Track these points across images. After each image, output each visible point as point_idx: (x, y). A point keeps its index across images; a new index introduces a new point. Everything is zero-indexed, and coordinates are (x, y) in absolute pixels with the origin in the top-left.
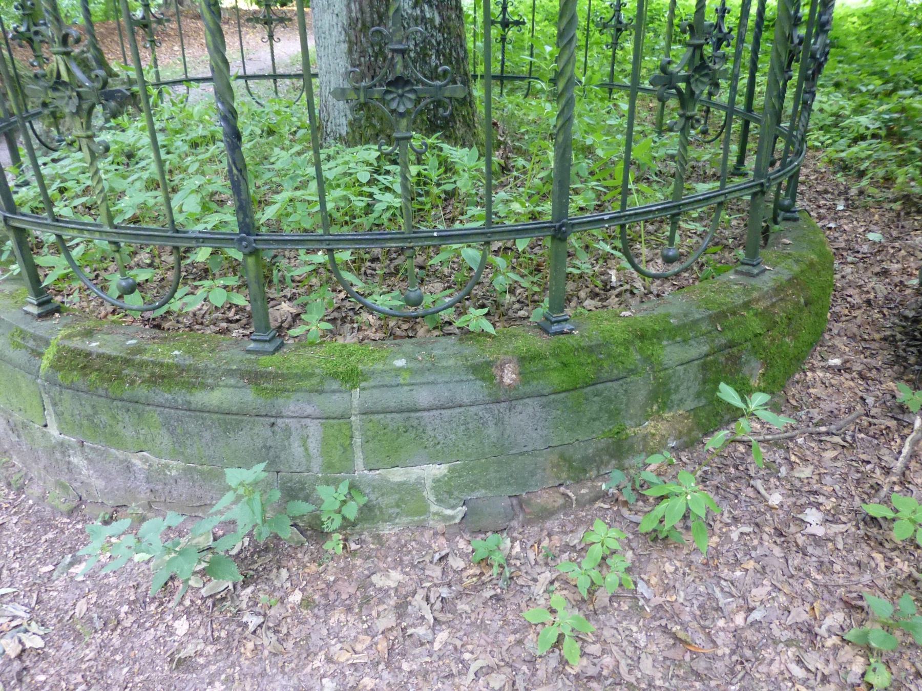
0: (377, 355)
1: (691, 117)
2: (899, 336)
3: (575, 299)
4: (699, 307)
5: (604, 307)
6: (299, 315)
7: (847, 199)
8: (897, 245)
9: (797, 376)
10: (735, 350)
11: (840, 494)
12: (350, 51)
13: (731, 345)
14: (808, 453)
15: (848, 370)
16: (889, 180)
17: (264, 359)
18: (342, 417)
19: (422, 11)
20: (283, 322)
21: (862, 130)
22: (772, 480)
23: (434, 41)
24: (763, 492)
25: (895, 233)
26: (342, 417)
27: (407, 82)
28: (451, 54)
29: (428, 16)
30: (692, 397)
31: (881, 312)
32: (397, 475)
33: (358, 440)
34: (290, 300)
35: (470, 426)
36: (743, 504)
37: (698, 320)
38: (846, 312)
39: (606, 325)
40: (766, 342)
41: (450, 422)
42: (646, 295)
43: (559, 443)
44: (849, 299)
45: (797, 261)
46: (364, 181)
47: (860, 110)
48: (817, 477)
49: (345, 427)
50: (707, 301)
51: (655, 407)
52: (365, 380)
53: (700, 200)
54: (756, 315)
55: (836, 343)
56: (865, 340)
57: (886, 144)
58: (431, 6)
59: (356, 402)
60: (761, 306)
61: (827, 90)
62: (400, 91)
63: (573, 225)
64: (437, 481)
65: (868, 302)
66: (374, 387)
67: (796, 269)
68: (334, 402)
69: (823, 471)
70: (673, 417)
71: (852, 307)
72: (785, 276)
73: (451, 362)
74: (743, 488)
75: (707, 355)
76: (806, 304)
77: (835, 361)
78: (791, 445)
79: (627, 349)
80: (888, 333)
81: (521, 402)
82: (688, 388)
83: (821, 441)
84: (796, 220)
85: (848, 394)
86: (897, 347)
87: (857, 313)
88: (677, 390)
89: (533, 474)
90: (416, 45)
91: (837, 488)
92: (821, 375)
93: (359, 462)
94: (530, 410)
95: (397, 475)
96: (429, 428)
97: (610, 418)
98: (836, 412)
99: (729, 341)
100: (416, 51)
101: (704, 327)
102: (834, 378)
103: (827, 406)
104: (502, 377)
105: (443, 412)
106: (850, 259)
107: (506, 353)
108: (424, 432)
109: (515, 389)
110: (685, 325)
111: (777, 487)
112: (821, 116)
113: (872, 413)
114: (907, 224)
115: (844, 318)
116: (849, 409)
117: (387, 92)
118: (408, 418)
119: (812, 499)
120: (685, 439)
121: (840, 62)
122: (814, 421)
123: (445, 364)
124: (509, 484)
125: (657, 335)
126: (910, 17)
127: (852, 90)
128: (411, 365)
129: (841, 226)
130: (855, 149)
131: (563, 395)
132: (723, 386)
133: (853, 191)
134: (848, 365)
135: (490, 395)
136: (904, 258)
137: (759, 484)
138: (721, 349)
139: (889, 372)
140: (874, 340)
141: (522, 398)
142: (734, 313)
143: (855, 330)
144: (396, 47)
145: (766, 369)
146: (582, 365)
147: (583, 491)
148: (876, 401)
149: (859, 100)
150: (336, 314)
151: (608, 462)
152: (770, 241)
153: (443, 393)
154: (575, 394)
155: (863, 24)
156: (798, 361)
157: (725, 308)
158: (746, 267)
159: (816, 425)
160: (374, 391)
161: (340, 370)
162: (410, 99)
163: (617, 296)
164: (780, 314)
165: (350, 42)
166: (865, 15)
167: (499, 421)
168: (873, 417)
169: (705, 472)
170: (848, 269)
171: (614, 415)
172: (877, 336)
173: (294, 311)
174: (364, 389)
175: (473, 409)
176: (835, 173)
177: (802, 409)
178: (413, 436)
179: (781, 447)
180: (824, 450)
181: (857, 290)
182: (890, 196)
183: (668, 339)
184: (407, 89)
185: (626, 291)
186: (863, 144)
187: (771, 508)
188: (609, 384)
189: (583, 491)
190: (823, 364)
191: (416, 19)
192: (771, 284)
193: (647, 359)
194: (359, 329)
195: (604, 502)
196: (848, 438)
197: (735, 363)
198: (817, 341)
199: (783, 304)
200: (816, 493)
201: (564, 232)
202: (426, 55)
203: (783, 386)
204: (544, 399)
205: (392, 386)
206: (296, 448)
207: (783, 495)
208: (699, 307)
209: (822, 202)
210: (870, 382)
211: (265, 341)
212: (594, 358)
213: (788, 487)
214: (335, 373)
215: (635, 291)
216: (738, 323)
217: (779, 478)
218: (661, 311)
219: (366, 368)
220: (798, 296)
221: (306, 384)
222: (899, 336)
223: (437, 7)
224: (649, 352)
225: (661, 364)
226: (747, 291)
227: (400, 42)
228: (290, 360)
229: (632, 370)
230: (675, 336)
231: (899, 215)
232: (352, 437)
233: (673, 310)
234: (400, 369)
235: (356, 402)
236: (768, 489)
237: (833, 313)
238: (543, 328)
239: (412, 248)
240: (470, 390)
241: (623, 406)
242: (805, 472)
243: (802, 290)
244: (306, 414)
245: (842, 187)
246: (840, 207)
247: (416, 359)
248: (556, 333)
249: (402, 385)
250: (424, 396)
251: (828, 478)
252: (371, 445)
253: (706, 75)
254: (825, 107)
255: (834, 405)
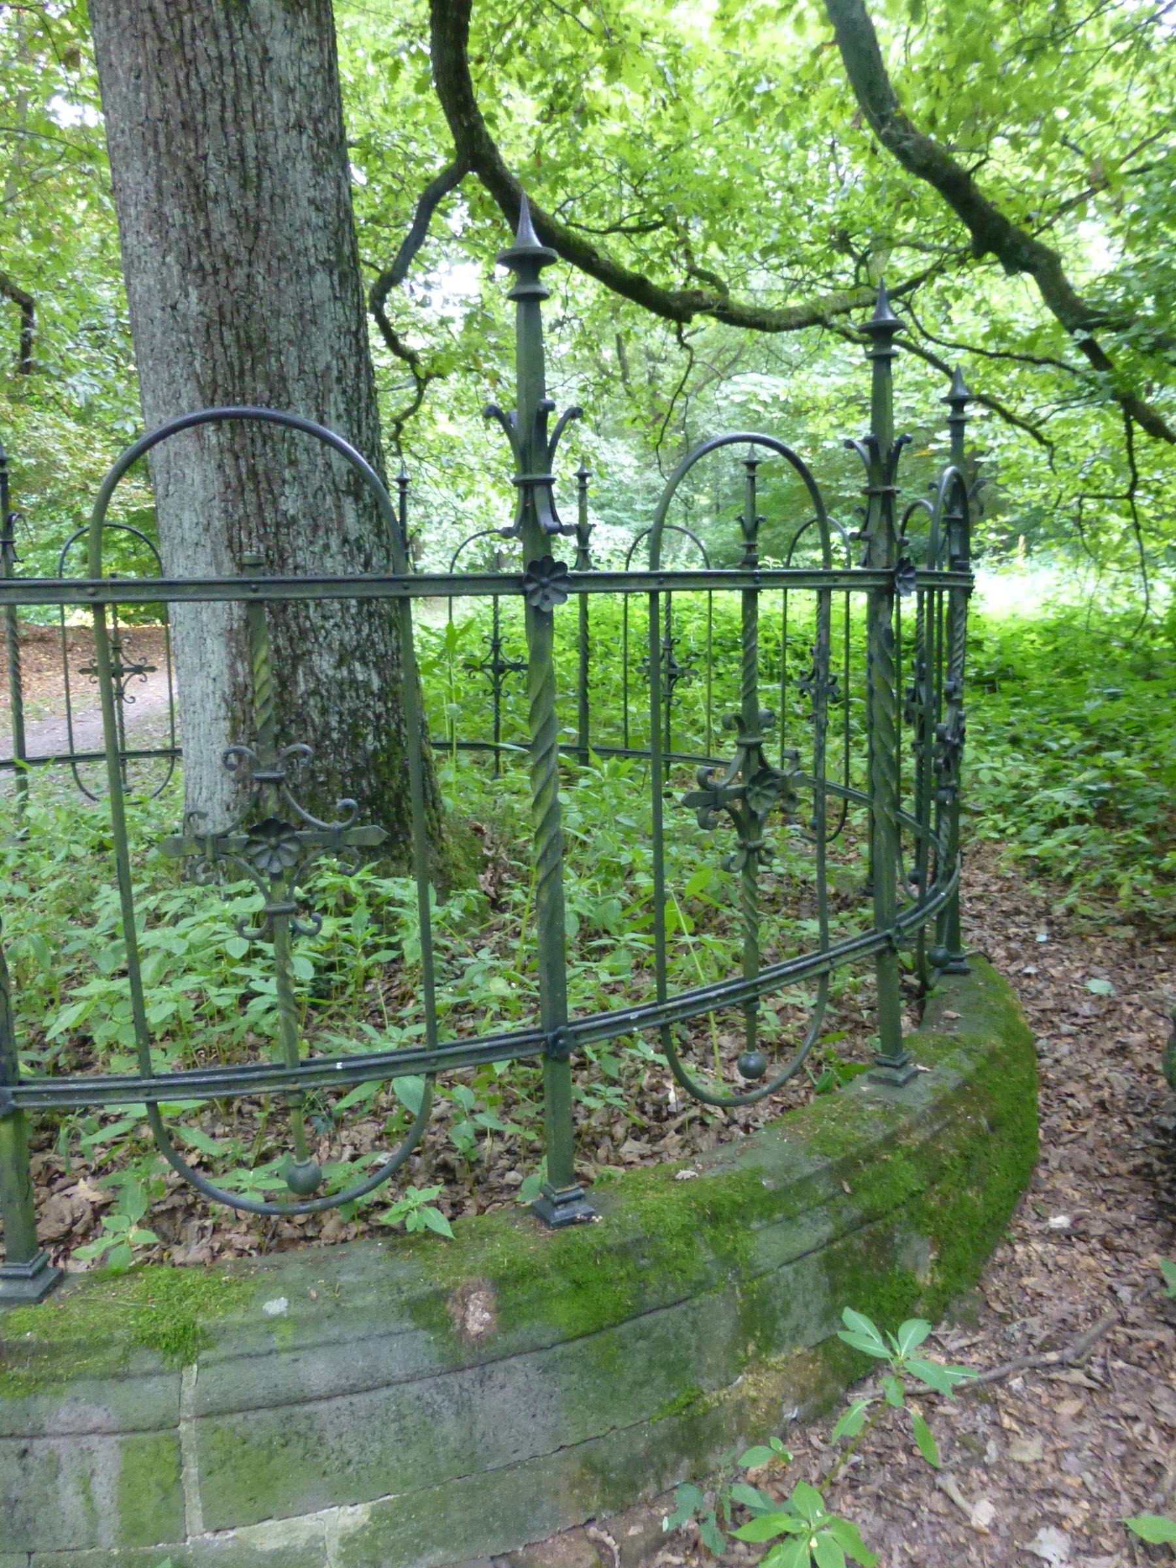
0: (234, 1293)
1: (757, 849)
2: (1157, 1166)
3: (607, 1141)
4: (810, 1152)
5: (654, 1155)
6: (106, 1205)
7: (1050, 923)
8: (1135, 998)
9: (1000, 1253)
10: (879, 1226)
11: (1094, 1491)
12: (234, 733)
13: (870, 1217)
14: (1031, 1408)
15: (1084, 1236)
16: (1108, 889)
17: (20, 1315)
18: (161, 1427)
19: (351, 672)
20: (74, 1222)
21: (1059, 810)
22: (974, 1472)
23: (370, 714)
24: (959, 1499)
25: (1130, 978)
26: (161, 1427)
27: (286, 827)
28: (399, 732)
29: (360, 677)
30: (815, 1320)
31: (1124, 1121)
32: (270, 1536)
33: (192, 1470)
34: (93, 1174)
35: (408, 1422)
36: (928, 1529)
37: (809, 1178)
38: (1069, 1127)
39: (651, 1199)
40: (933, 1204)
41: (370, 1417)
42: (727, 1126)
43: (579, 1437)
44: (1071, 1102)
45: (969, 1052)
46: (238, 955)
47: (1053, 778)
48: (1050, 1458)
49: (166, 1446)
50: (826, 1140)
51: (751, 1347)
52: (209, 1347)
53: (789, 974)
54: (908, 1157)
55: (1058, 1185)
56: (1103, 1176)
57: (1096, 831)
58: (365, 664)
59: (189, 1394)
60: (918, 1137)
61: (999, 749)
62: (273, 841)
63: (577, 1035)
64: (348, 1541)
65: (1101, 1104)
66: (228, 1359)
67: (969, 1066)
68: (146, 1397)
69: (1061, 1444)
70: (786, 1362)
71: (1078, 1115)
72: (951, 1081)
73: (371, 1298)
74: (924, 1494)
75: (831, 1241)
76: (992, 1128)
77: (1060, 1221)
78: (1001, 1394)
79: (689, 1244)
80: (1139, 1161)
81: (501, 1364)
82: (806, 1305)
83: (1052, 1381)
84: (966, 972)
85: (1088, 1283)
86: (1156, 1185)
87: (1086, 1126)
88: (786, 1312)
89: (534, 1504)
90: (341, 722)
91: (1088, 1478)
92: (1040, 1248)
93: (195, 1517)
94: (520, 1380)
95: (270, 1536)
96: (329, 1435)
97: (670, 1377)
98: (1071, 1320)
99: (866, 1210)
100: (341, 731)
101: (821, 1189)
102: (1060, 1251)
103: (1054, 1309)
104: (464, 1320)
105: (355, 1399)
106: (1065, 1028)
107: (470, 1273)
108: (320, 1441)
109: (489, 1342)
110: (787, 1189)
111: (984, 1486)
112: (996, 790)
113: (1131, 1318)
114: (1147, 961)
115: (1066, 1138)
116: (1092, 1311)
117: (250, 843)
118: (290, 1417)
119: (1047, 1507)
120: (813, 1400)
121: (1015, 705)
122: (1036, 1342)
123: (359, 1303)
124: (491, 1531)
125: (741, 1212)
126: (1110, 633)
127: (1040, 748)
128: (297, 1310)
129: (1045, 970)
130: (1049, 843)
131: (579, 1343)
132: (850, 1316)
133: (1059, 909)
134: (1081, 1226)
135: (442, 1357)
136: (1149, 1021)
137: (949, 1482)
138: (855, 1226)
139: (1149, 1234)
140: (1118, 1175)
141: (503, 1358)
142: (870, 1159)
143: (1085, 1157)
144: (266, 775)
145: (941, 1252)
146: (610, 1281)
147: (633, 1531)
148: (1134, 1295)
149: (1050, 761)
150: (177, 1200)
151: (676, 1464)
152: (926, 1013)
153: (358, 1362)
154: (600, 1339)
155: (1045, 644)
156: (996, 1227)
157: (853, 1150)
158: (886, 1070)
159: (1042, 1349)
160: (226, 1367)
161: (162, 1329)
162: (289, 852)
163: (678, 1131)
164: (948, 1152)
165: (233, 718)
166: (1047, 630)
167: (463, 1408)
168: (1134, 1325)
169: (855, 1467)
170: (1064, 1047)
171: (676, 1370)
172: (1123, 1167)
173: (98, 1197)
174: (205, 1365)
175: (414, 1389)
176: (1028, 879)
177: (1014, 1319)
178: (299, 1451)
179: (984, 1400)
180: (1060, 1399)
181: (1083, 1084)
182: (1116, 915)
183: (761, 1216)
184: (285, 836)
185: (692, 1120)
186: (1062, 834)
187: (978, 1533)
188: (663, 1314)
189: (633, 1531)
190: (1039, 1226)
191: (341, 684)
192: (929, 1098)
193: (727, 1260)
194: (216, 1229)
195: (673, 1552)
196: (1097, 1372)
197: (882, 1250)
198: (1024, 1180)
199: (951, 1133)
200: (1051, 1493)
201: (563, 1047)
202: (357, 735)
203: (979, 1277)
204: (545, 1356)
205: (258, 1355)
206: (70, 1500)
207: (994, 1502)
208: (810, 1152)
209: (1013, 930)
210: (1121, 1255)
211: (25, 1278)
212: (630, 1267)
213: (1004, 1483)
214: (153, 1336)
215: (709, 1120)
216: (880, 1176)
217: (986, 1468)
218: (745, 1163)
219: (211, 1322)
220: (976, 1116)
221: (96, 1363)
222: (1157, 1166)
223: (375, 665)
224: (729, 1247)
225: (751, 1265)
226: (889, 1115)
227: (273, 768)
228: (74, 1314)
229: (700, 1283)
230: (771, 1211)
231: (1132, 946)
232: (180, 1465)
233: (767, 1160)
234: (276, 1319)
235: (189, 1394)
236: (968, 1493)
237: (1049, 1130)
238: (540, 1215)
239: (299, 1091)
240: (406, 1351)
241: (692, 1353)
242: (1029, 1450)
243: (982, 1102)
244: (90, 1426)
245: (1041, 903)
246: (1042, 938)
247: (305, 1296)
248: (562, 1224)
249: (278, 1352)
250: (318, 1372)
251: (1071, 1458)
252: (218, 1479)
253: (770, 787)
254: (1000, 776)
255: (1065, 1306)
